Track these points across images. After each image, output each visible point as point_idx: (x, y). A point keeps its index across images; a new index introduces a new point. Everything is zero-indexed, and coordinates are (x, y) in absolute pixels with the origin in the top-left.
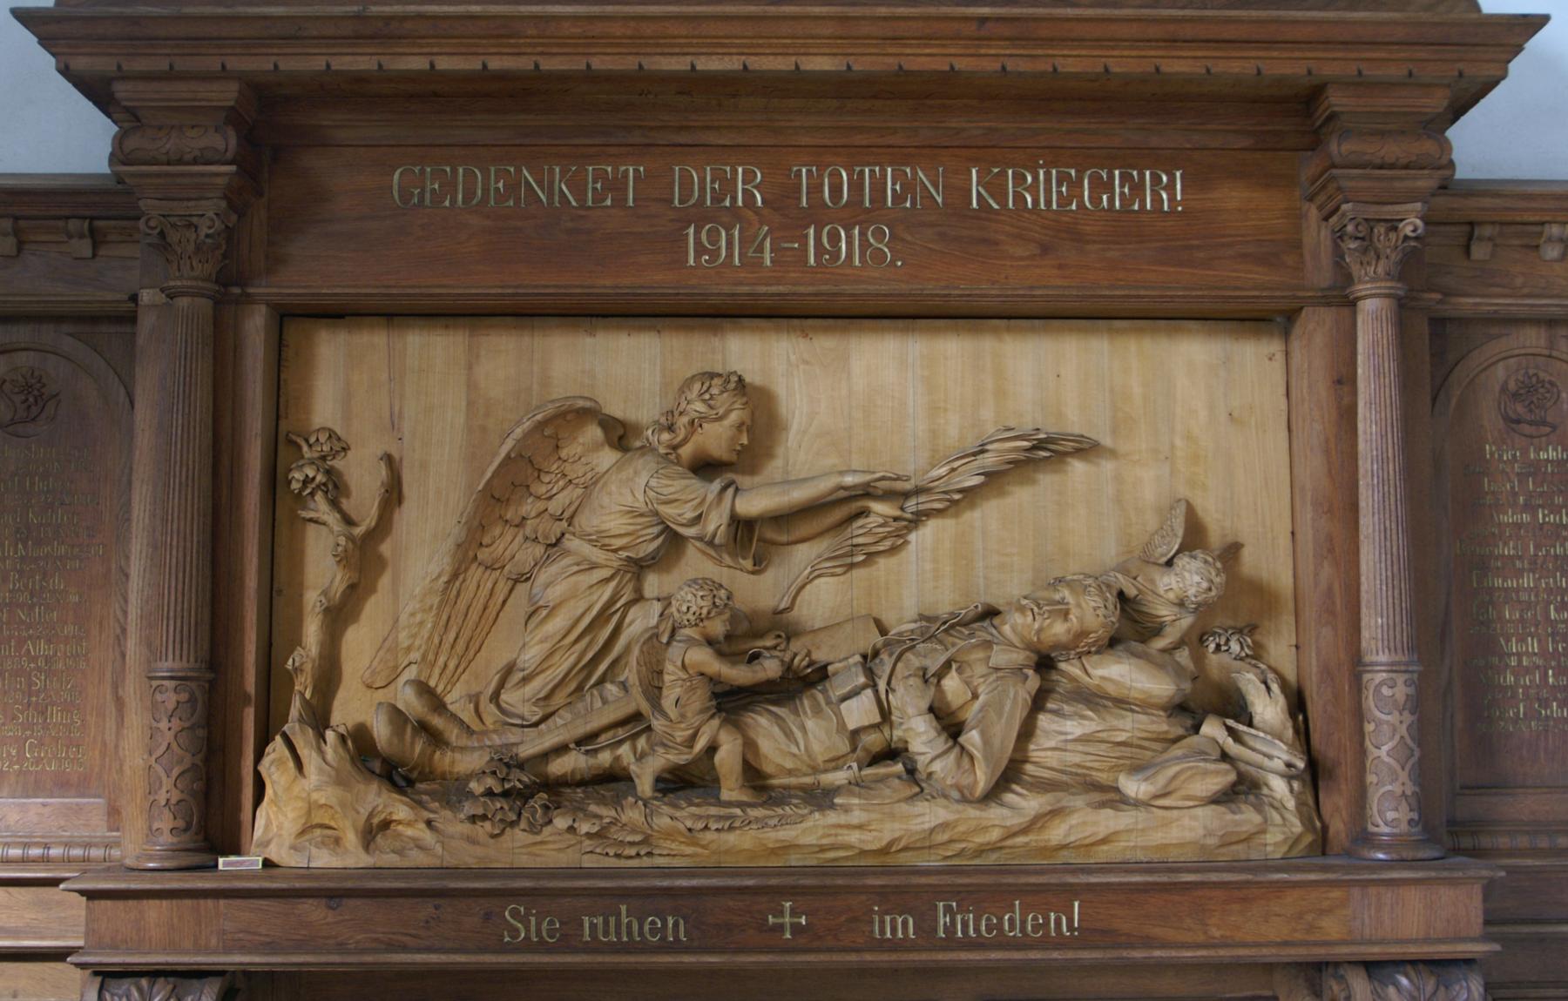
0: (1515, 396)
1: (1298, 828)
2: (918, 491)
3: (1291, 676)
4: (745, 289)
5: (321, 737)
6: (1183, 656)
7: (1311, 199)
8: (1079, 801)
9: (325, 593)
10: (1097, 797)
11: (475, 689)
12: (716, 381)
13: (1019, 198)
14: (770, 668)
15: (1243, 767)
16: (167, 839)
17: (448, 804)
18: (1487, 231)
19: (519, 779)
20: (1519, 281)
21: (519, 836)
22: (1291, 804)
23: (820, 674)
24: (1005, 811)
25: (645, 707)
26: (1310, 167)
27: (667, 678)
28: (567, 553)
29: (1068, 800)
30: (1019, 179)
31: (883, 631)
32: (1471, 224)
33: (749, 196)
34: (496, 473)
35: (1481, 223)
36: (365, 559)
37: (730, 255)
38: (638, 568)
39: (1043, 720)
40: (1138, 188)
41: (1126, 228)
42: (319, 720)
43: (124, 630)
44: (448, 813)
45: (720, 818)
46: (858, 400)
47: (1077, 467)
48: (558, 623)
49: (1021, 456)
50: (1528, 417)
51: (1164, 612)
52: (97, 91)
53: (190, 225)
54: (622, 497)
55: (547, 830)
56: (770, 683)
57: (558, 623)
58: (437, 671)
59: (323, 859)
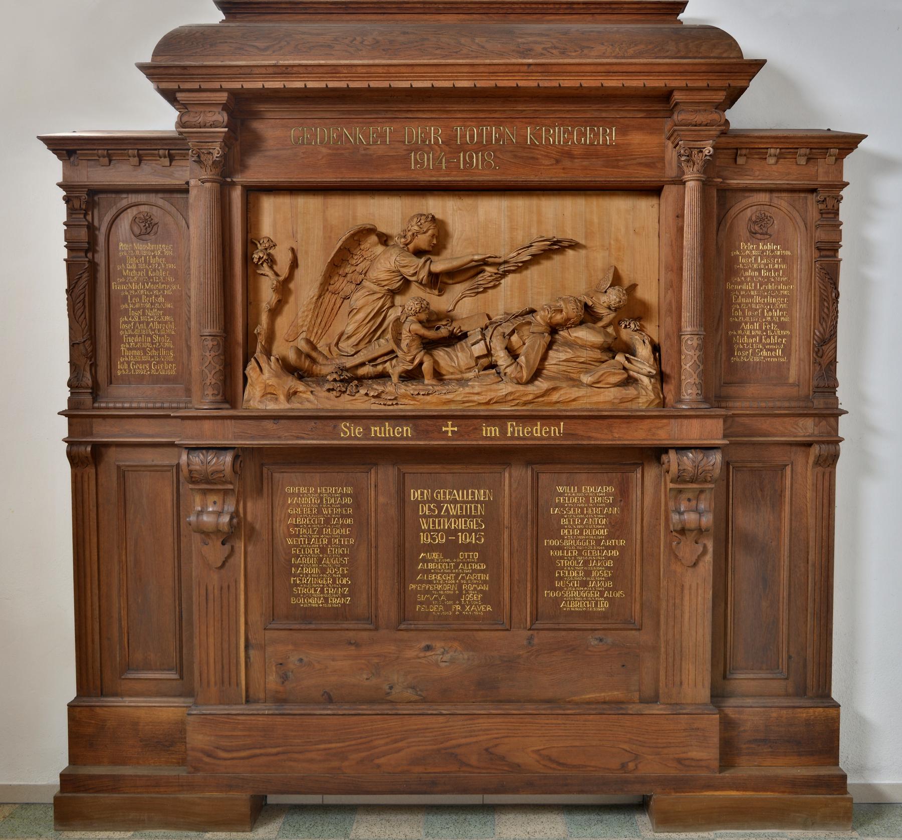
0: (755, 222)
1: (653, 397)
2: (505, 262)
3: (656, 339)
4: (434, 179)
5: (269, 359)
6: (610, 330)
7: (669, 139)
8: (564, 385)
9: (268, 303)
10: (571, 383)
11: (329, 341)
12: (423, 217)
13: (547, 139)
14: (444, 332)
15: (631, 373)
16: (210, 398)
17: (318, 384)
18: (744, 152)
19: (346, 375)
20: (757, 173)
21: (345, 397)
22: (650, 388)
23: (465, 335)
24: (535, 388)
25: (395, 348)
26: (668, 125)
27: (403, 336)
28: (364, 287)
29: (558, 384)
30: (548, 131)
31: (490, 319)
32: (737, 149)
33: (436, 139)
34: (335, 255)
35: (741, 149)
36: (284, 289)
37: (428, 165)
38: (393, 293)
39: (551, 353)
40: (597, 135)
41: (591, 152)
42: (268, 353)
43: (189, 319)
44: (319, 388)
45: (423, 390)
46: (479, 225)
47: (570, 253)
48: (361, 316)
49: (547, 248)
50: (761, 231)
51: (602, 311)
52: (170, 96)
53: (209, 153)
54: (385, 264)
55: (357, 395)
56: (444, 338)
57: (361, 316)
58: (314, 335)
59: (271, 406)
